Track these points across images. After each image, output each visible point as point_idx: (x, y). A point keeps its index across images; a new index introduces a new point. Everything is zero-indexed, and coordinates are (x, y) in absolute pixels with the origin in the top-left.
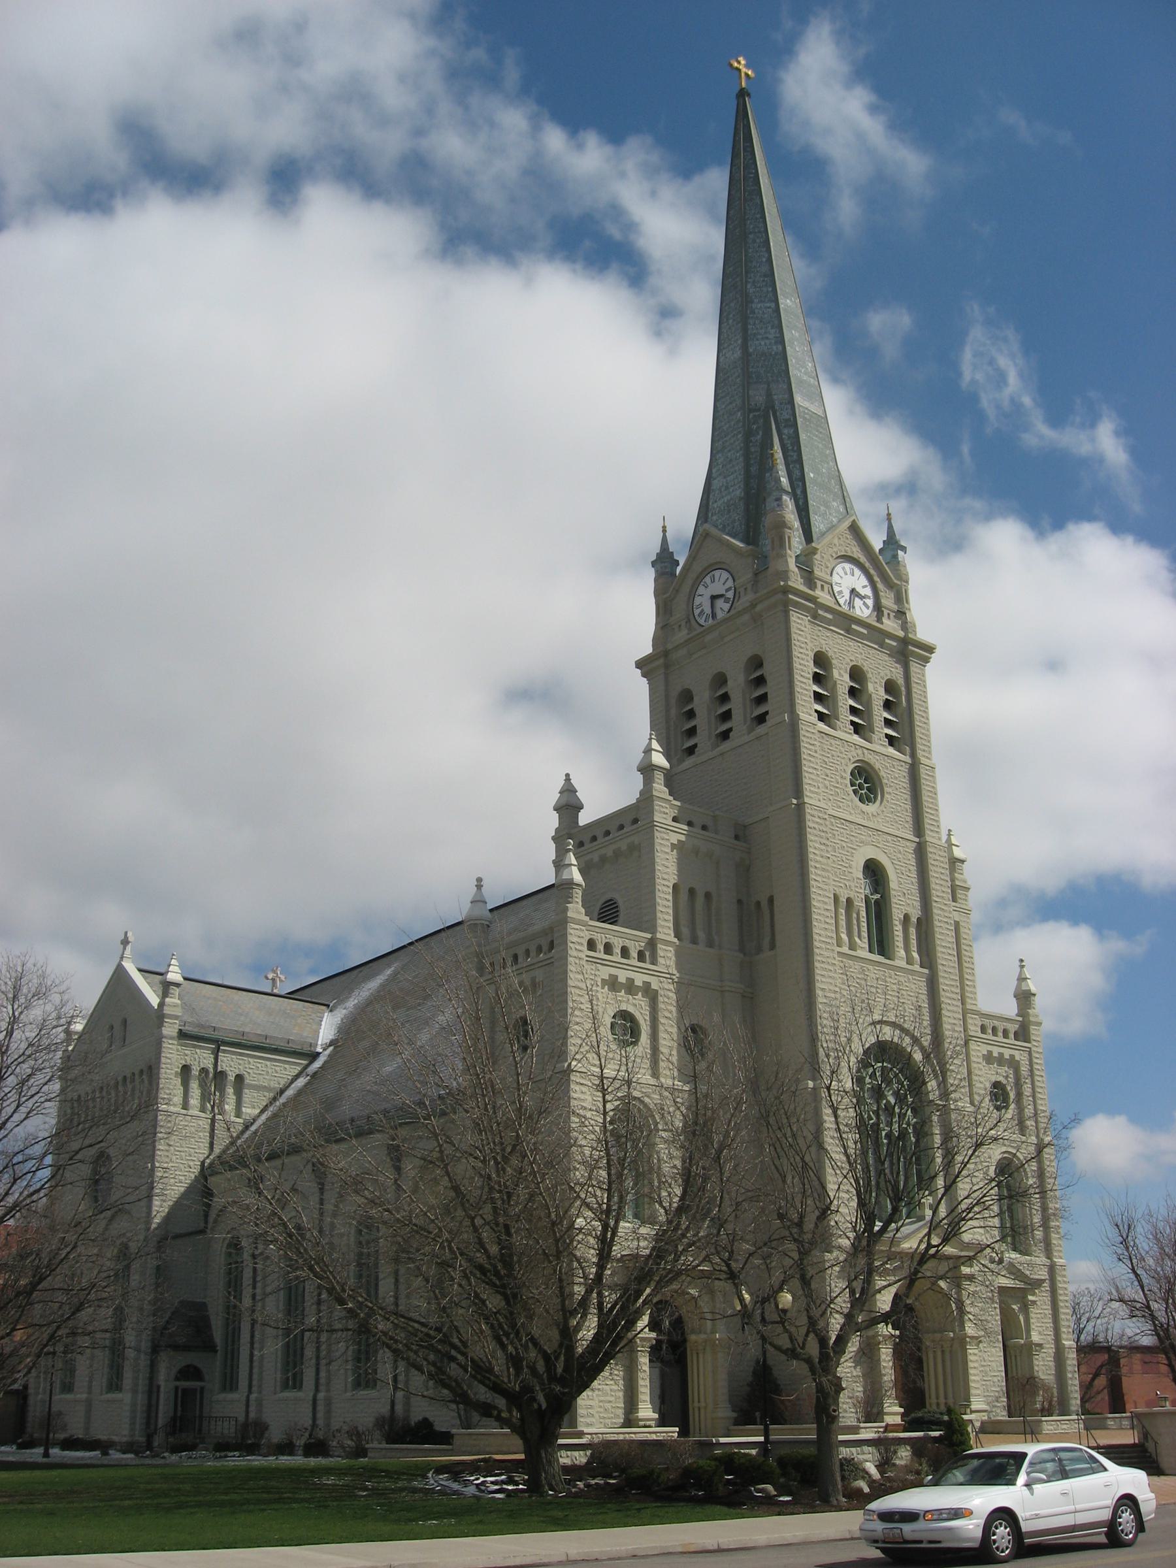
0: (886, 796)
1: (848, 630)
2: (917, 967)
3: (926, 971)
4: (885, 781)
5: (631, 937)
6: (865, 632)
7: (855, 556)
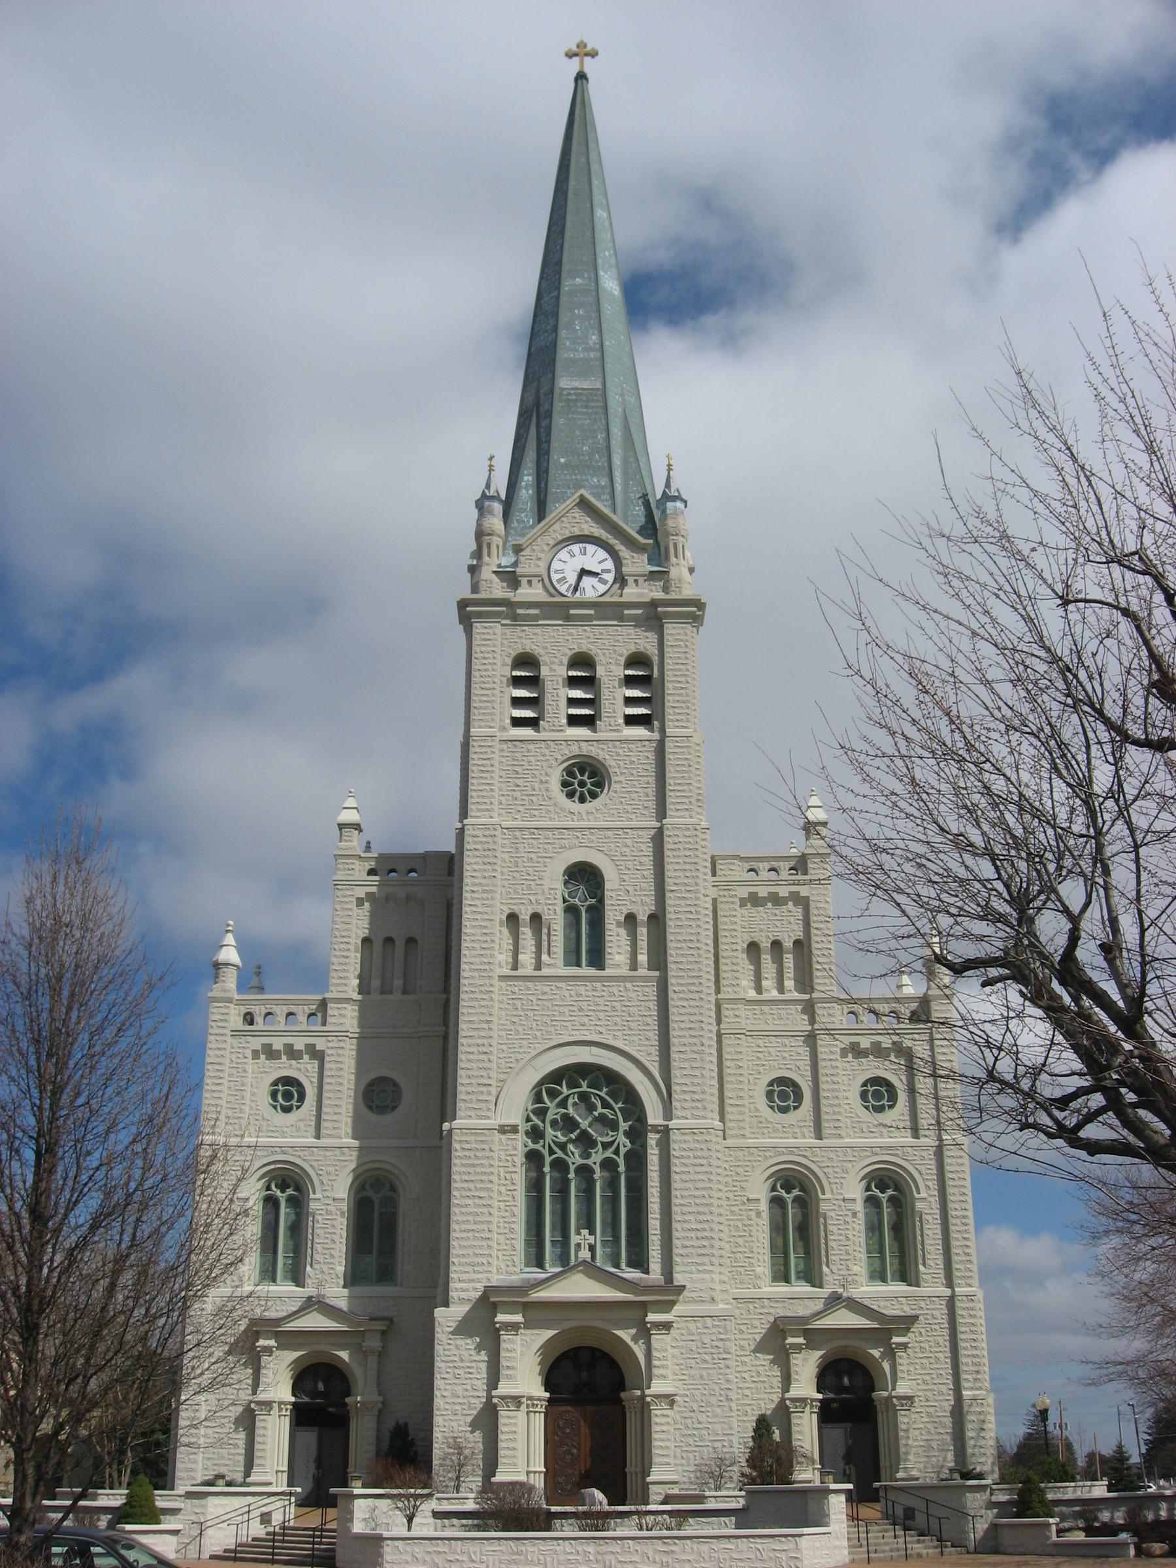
0: (613, 785)
1: (568, 618)
2: (642, 972)
3: (657, 973)
4: (611, 770)
5: (297, 1002)
6: (592, 612)
7: (587, 533)
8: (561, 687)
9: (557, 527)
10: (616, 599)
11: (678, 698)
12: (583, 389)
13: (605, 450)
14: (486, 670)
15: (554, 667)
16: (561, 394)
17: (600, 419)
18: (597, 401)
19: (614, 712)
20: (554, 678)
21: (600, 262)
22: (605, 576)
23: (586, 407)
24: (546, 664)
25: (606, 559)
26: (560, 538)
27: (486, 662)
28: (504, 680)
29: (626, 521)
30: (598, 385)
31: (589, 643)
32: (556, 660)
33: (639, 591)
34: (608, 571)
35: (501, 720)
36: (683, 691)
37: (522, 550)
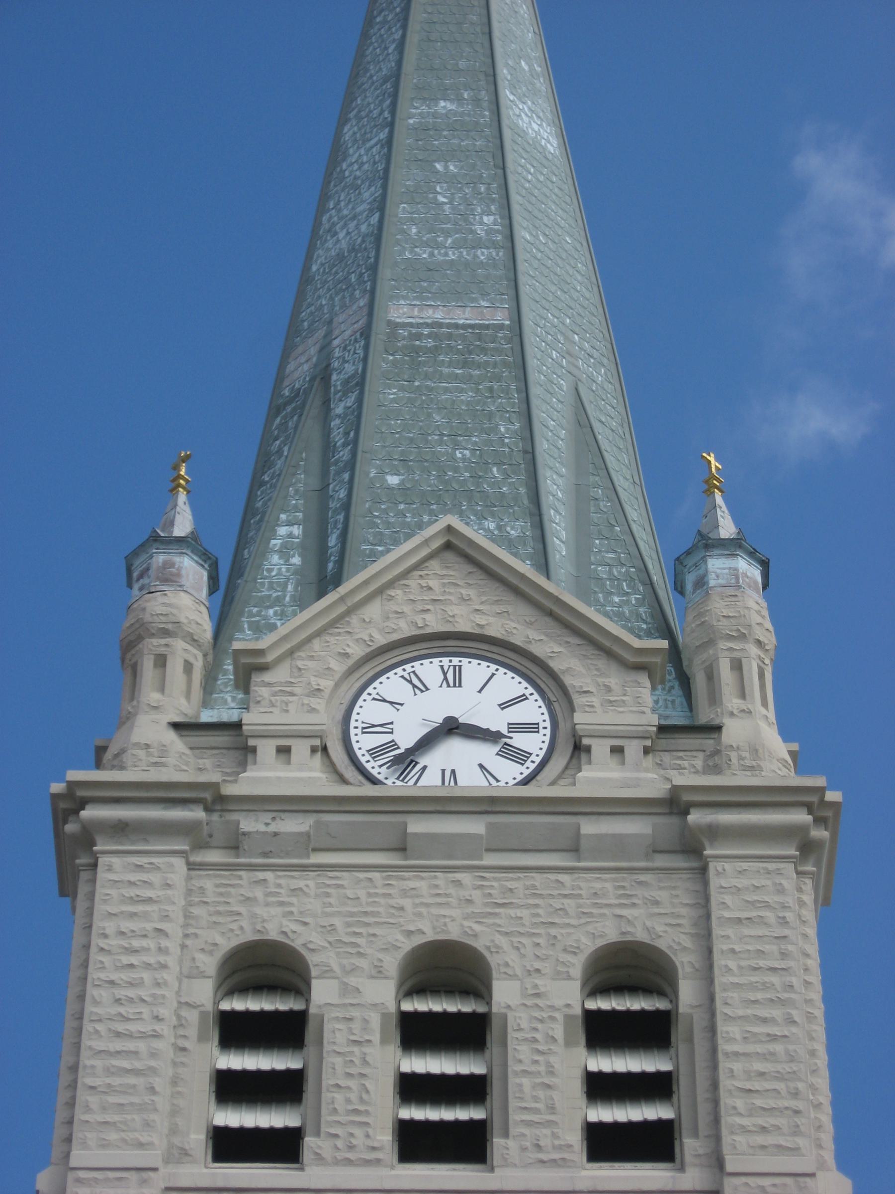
8: (376, 1038)
9: (374, 610)
10: (561, 791)
11: (759, 1066)
12: (457, 326)
13: (519, 458)
14: (131, 984)
15: (353, 981)
16: (393, 336)
17: (507, 391)
18: (498, 351)
19: (552, 1109)
20: (355, 1013)
21: (503, 72)
22: (520, 741)
23: (465, 364)
24: (329, 972)
25: (523, 698)
26: (381, 640)
27: (134, 960)
28: (193, 1017)
29: (584, 594)
30: (501, 317)
31: (467, 917)
32: (363, 963)
33: (628, 775)
34: (532, 728)
35: (174, 1131)
36: (778, 1048)
37: (263, 668)
